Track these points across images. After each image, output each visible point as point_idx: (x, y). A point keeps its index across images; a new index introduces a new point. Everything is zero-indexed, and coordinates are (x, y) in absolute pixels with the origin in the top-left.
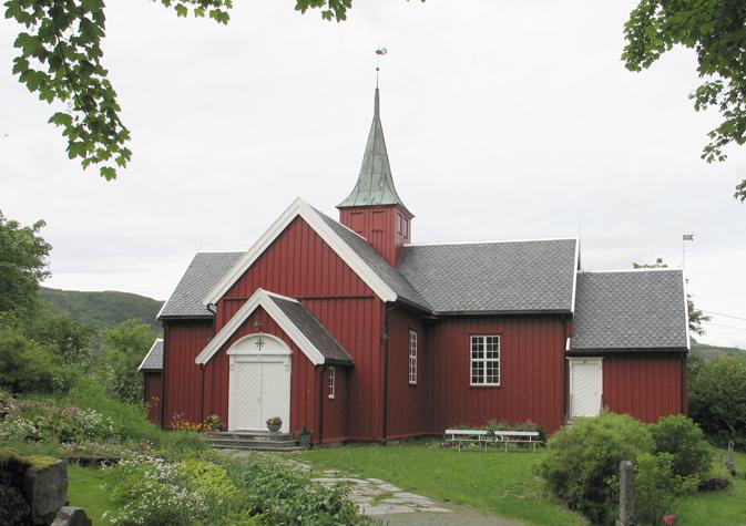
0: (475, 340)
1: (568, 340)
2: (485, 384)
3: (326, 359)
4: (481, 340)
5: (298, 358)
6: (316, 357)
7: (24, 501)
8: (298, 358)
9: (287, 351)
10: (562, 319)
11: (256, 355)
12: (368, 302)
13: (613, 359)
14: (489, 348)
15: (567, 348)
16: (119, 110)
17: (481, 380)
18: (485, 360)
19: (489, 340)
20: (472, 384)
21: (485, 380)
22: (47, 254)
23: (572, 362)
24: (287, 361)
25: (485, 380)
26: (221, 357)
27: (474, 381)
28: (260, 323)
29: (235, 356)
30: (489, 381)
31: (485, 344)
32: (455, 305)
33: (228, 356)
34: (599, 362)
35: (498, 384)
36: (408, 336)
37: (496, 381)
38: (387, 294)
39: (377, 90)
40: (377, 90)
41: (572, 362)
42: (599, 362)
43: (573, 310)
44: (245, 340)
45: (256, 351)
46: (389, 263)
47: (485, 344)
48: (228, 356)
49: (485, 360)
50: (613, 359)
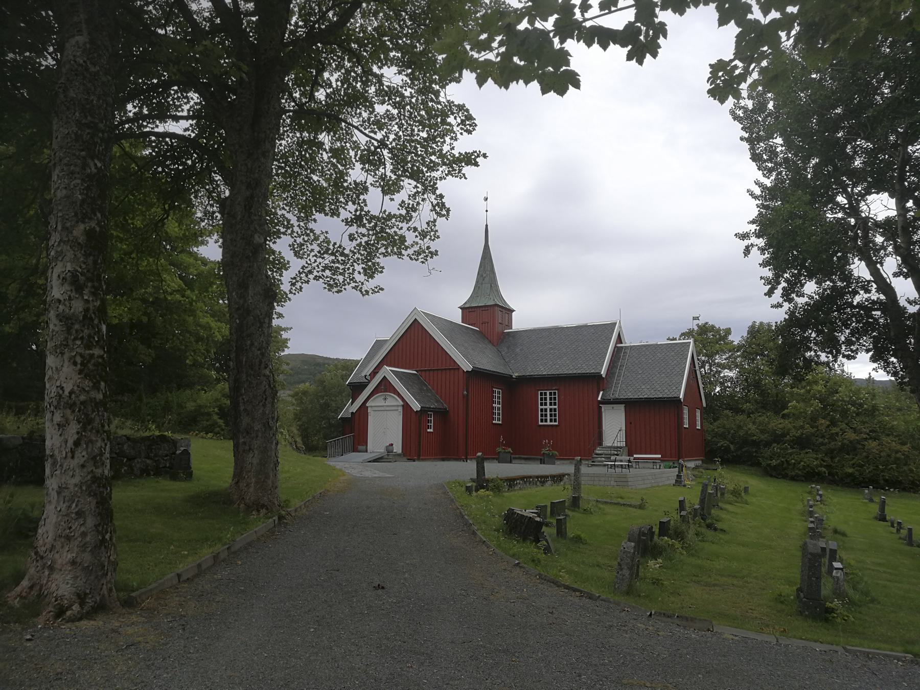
0: (541, 394)
1: (601, 393)
2: (549, 423)
3: (422, 407)
4: (545, 394)
5: (406, 407)
6: (416, 406)
7: (607, 604)
8: (406, 407)
9: (402, 403)
10: (595, 380)
11: (383, 406)
12: (456, 371)
13: (633, 406)
14: (551, 399)
15: (599, 399)
16: (665, 37)
17: (546, 421)
18: (548, 407)
19: (550, 394)
20: (540, 423)
21: (548, 420)
22: (287, 347)
23: (604, 407)
24: (400, 409)
25: (548, 420)
26: (363, 407)
27: (542, 421)
28: (385, 386)
29: (371, 407)
30: (551, 421)
31: (548, 396)
32: (530, 371)
33: (367, 407)
34: (622, 407)
35: (557, 423)
36: (493, 392)
37: (555, 421)
38: (466, 366)
39: (487, 226)
40: (487, 226)
41: (604, 407)
42: (622, 407)
43: (603, 372)
44: (377, 397)
45: (382, 403)
46: (493, 345)
47: (548, 396)
48: (367, 407)
49: (548, 407)
50: (633, 406)
